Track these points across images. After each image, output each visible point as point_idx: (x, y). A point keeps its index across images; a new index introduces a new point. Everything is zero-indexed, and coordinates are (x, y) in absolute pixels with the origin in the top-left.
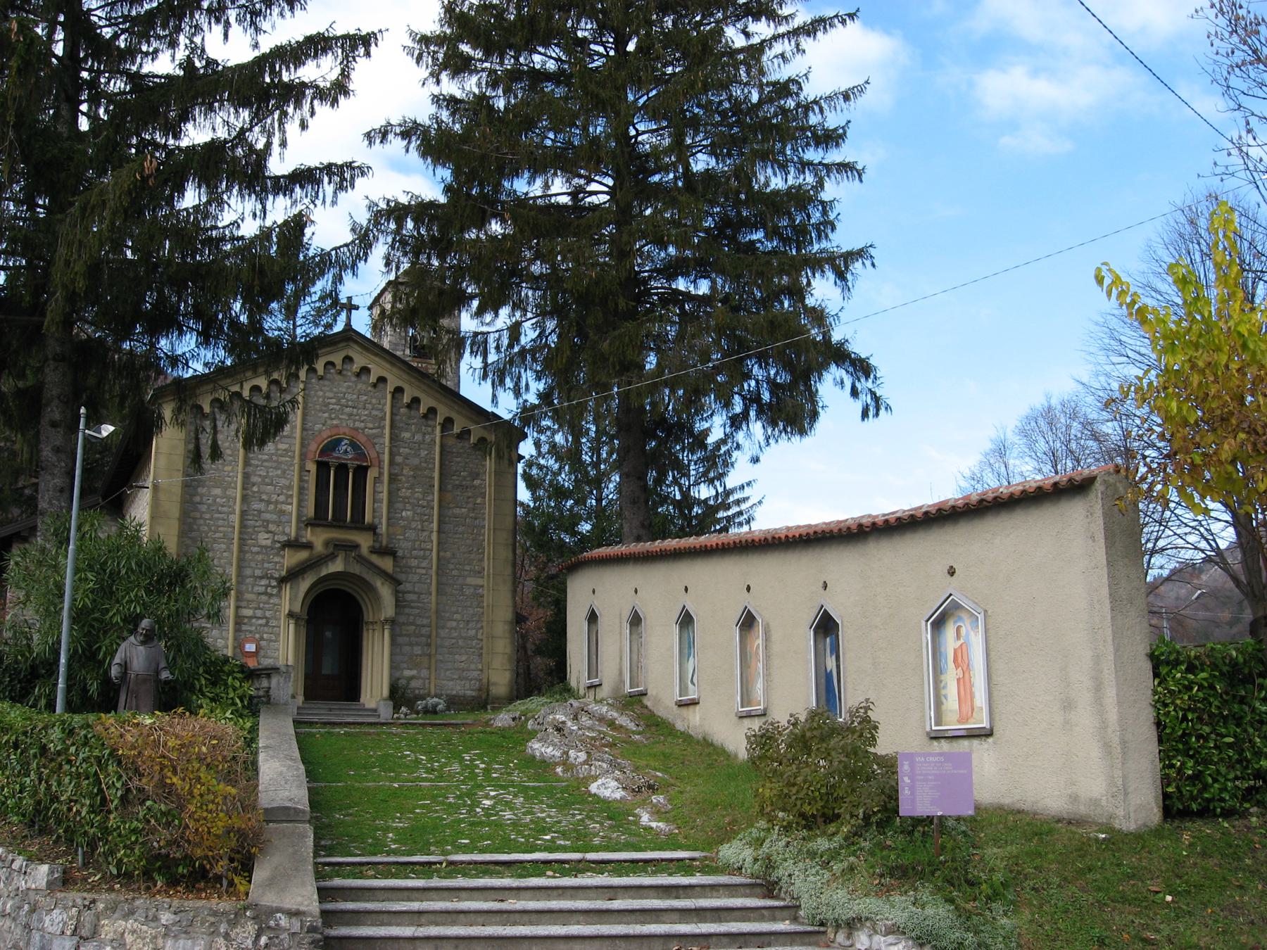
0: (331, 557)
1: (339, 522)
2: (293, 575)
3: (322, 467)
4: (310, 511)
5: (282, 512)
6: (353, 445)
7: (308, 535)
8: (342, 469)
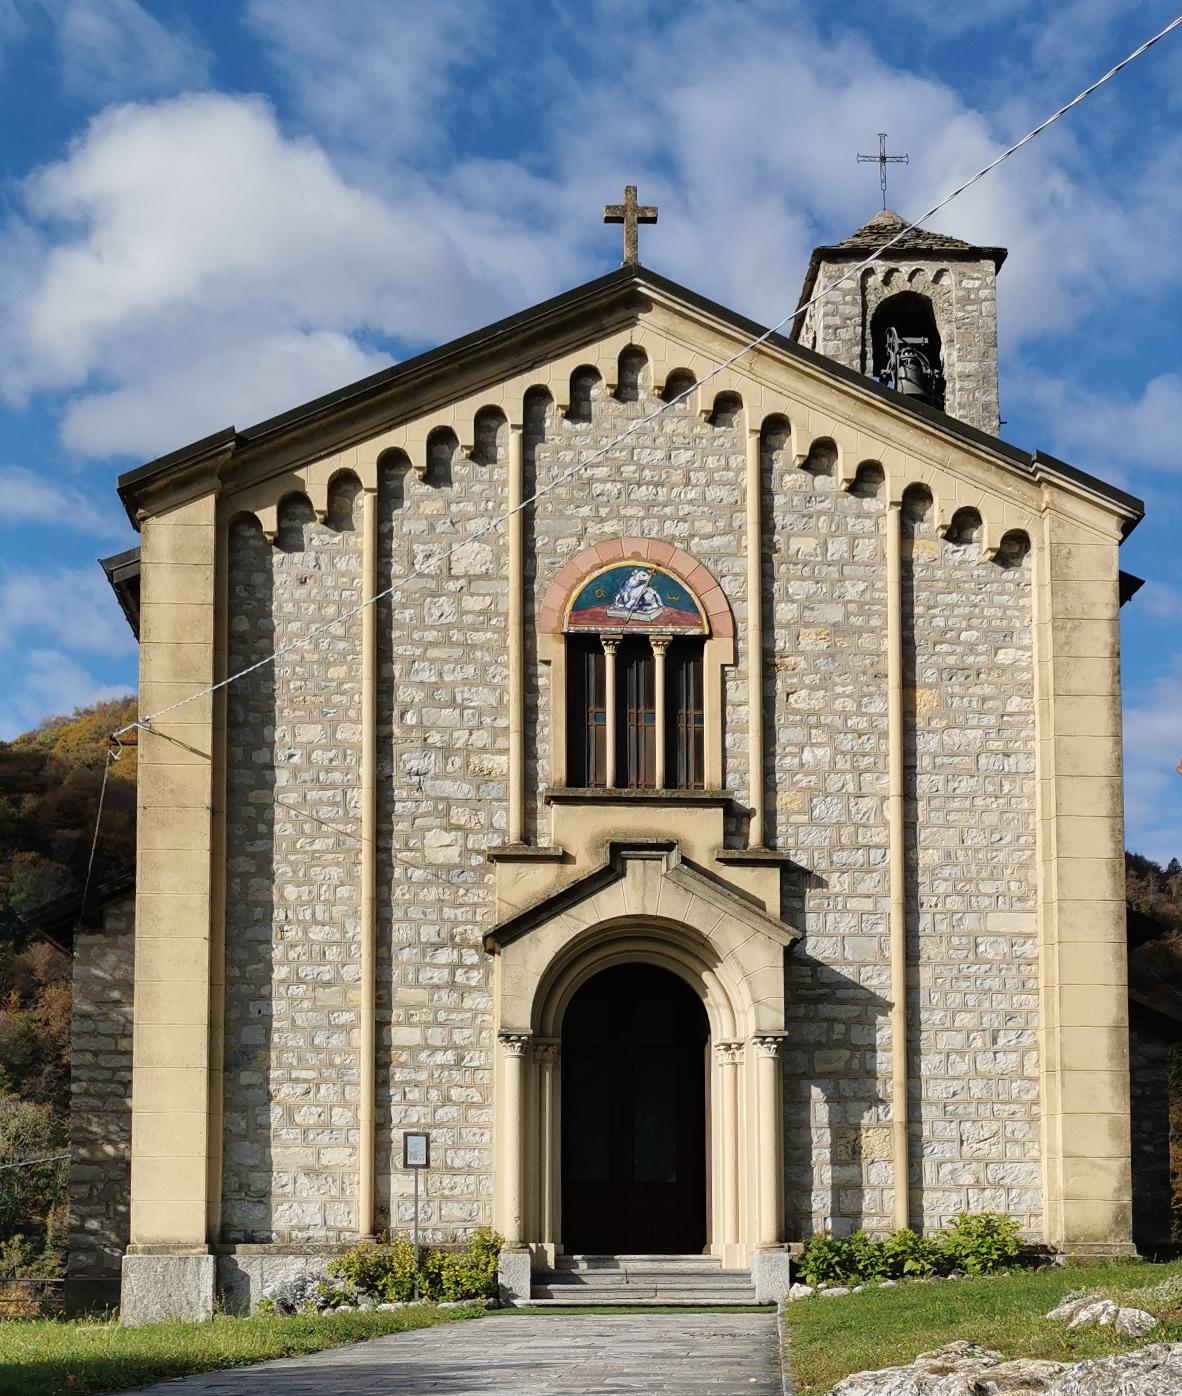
0: (611, 873)
1: (627, 791)
2: (504, 935)
3: (581, 648)
4: (553, 764)
5: (484, 777)
6: (664, 584)
7: (558, 826)
8: (634, 648)
